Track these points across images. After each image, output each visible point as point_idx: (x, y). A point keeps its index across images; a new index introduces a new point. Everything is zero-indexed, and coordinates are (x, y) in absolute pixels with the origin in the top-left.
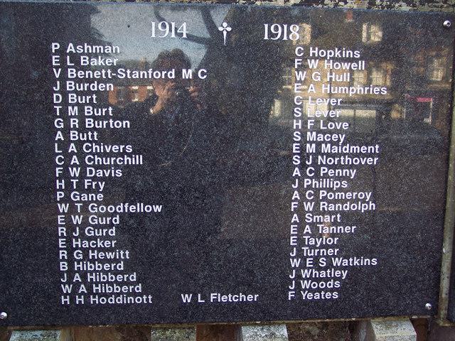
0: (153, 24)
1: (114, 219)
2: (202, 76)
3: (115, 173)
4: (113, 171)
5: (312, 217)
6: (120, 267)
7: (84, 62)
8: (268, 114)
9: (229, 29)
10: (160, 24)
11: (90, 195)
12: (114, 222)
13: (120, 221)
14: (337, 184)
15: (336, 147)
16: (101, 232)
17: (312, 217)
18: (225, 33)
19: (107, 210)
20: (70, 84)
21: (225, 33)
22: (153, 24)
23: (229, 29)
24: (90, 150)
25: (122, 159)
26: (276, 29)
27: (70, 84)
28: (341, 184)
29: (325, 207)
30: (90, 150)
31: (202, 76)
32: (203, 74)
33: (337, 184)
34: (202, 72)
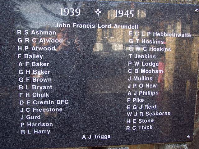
0: (62, 9)
1: (38, 117)
2: (28, 111)
3: (42, 125)
4: (41, 124)
5: (149, 113)
6: (39, 118)
7: (34, 80)
8: (182, 23)
9: (100, 12)
10: (65, 9)
11: (47, 87)
12: (38, 118)
13: (32, 63)
14: (154, 93)
15: (157, 71)
16: (34, 117)
17: (149, 113)
18: (98, 14)
19: (47, 48)
20: (34, 86)
21: (98, 14)
22: (62, 9)
23: (100, 12)
24: (36, 96)
25: (89, 25)
26: (121, 12)
27: (34, 86)
28: (156, 93)
29: (147, 107)
30: (36, 96)
31: (28, 111)
32: (28, 110)
33: (154, 93)
34: (35, 101)
